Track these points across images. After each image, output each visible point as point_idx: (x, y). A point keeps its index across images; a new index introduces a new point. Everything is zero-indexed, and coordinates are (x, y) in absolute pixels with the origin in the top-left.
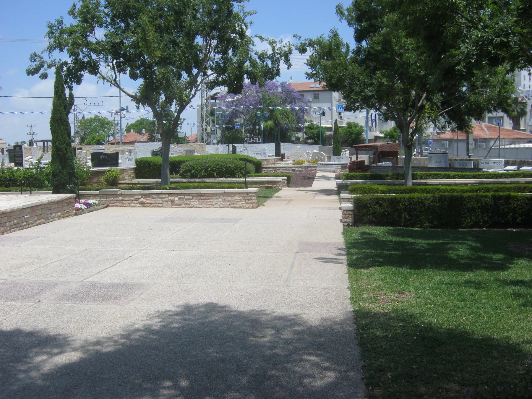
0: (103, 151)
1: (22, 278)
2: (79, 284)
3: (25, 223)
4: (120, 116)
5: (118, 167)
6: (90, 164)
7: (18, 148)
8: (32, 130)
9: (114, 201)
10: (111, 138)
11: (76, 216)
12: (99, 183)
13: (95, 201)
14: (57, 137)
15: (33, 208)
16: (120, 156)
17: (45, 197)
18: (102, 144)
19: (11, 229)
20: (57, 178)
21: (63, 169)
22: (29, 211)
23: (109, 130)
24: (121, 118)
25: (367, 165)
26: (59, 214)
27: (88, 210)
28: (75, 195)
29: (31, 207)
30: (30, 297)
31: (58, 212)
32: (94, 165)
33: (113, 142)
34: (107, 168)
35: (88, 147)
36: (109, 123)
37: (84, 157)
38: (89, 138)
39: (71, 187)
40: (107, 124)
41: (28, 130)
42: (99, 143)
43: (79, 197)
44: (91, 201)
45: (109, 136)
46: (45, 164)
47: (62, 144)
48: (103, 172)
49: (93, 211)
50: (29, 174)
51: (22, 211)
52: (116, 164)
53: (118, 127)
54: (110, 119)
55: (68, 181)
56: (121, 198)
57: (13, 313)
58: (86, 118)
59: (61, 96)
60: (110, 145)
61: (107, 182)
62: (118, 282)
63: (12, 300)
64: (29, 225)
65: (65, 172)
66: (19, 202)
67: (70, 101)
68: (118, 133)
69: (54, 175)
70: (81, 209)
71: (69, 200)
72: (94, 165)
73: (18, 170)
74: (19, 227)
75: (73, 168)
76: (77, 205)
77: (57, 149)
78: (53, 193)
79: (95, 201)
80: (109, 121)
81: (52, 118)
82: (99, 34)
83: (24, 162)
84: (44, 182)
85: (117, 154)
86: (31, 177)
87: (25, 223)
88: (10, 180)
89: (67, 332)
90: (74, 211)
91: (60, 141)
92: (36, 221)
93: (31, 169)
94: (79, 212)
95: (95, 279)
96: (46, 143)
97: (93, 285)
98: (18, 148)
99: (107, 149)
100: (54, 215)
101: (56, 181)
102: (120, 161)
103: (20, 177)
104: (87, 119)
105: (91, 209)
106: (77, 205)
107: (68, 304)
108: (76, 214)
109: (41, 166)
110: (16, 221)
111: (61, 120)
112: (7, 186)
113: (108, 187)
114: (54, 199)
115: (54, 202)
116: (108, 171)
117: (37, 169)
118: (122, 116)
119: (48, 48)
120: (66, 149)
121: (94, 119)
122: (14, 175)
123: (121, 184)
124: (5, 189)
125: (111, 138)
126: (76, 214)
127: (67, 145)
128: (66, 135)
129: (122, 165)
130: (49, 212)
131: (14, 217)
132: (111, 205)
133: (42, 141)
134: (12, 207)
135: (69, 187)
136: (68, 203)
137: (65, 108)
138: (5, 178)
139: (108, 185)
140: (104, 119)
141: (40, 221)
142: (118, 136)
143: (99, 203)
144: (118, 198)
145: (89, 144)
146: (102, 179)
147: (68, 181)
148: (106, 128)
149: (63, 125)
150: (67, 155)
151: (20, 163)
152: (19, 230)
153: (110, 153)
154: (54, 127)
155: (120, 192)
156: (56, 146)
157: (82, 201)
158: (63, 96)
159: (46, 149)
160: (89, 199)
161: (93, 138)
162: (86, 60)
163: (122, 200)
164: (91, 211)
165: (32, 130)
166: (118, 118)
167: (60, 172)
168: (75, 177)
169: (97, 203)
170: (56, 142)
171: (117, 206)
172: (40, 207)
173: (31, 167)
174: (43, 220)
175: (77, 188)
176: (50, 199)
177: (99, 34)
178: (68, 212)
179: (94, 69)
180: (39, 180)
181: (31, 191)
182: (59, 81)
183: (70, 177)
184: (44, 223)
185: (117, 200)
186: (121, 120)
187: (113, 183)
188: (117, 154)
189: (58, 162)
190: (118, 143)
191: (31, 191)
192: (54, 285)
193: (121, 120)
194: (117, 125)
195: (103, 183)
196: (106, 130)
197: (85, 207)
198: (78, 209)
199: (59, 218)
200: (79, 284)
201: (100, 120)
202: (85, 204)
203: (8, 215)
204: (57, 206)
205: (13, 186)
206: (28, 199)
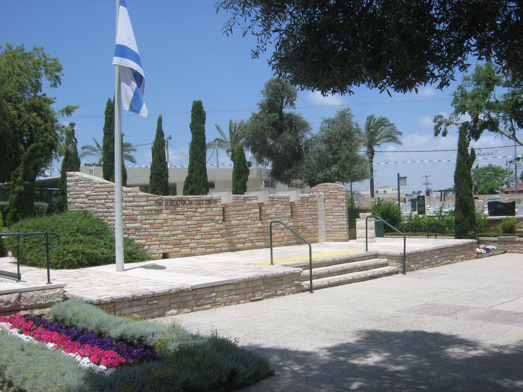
0: (499, 200)
1: (440, 302)
2: (486, 310)
3: (434, 262)
4: (516, 165)
5: (514, 215)
6: (486, 212)
7: (421, 198)
8: (427, 180)
9: (512, 248)
10: (505, 187)
11: (477, 260)
12: (496, 230)
13: (493, 247)
14: (460, 189)
15: (441, 250)
16: (516, 205)
17: (450, 241)
18: (496, 193)
19: (423, 267)
20: (460, 225)
21: (465, 217)
22: (437, 252)
23: (503, 178)
24: (516, 167)
25: (33, 204)
26: (463, 256)
27: (488, 254)
28: (476, 240)
29: (440, 249)
30: (450, 315)
31: (461, 255)
32: (491, 214)
33: (507, 190)
34: (504, 217)
35: (482, 196)
36: (503, 171)
37: (481, 205)
38: (482, 187)
39: (472, 234)
40: (501, 172)
41: (424, 180)
42: (492, 192)
43: (479, 242)
44: (490, 247)
45: (503, 185)
46: (445, 213)
47: (465, 195)
48: (500, 221)
49: (492, 255)
50: (433, 221)
51: (433, 251)
52: (513, 213)
53: (513, 176)
54: (504, 168)
55: (469, 228)
56: (518, 245)
57: (438, 323)
58: (479, 167)
59: (463, 152)
60: (504, 194)
61: (504, 230)
62: (520, 311)
63: (435, 315)
64: (437, 264)
65: (467, 219)
66: (429, 245)
67: (472, 157)
68: (512, 181)
69: (457, 222)
70: (481, 253)
71: (471, 245)
72: (491, 214)
73: (423, 218)
74: (429, 265)
75: (474, 216)
76: (478, 250)
77: (460, 199)
78: (455, 238)
79: (493, 247)
80: (503, 170)
81: (456, 173)
82: (500, 93)
83: (426, 211)
84: (445, 229)
85: (514, 203)
86: (434, 224)
87: (434, 262)
88: (417, 226)
89: (481, 339)
90: (475, 255)
91: (463, 192)
92: (443, 261)
93: (434, 217)
94: (479, 256)
95: (500, 308)
96: (443, 193)
97: (498, 312)
98: (421, 198)
99: (503, 198)
100: (458, 257)
101: (459, 227)
102: (516, 210)
103: (425, 223)
104: (481, 168)
105: (490, 253)
106: (478, 250)
107: (480, 322)
108: (477, 257)
109: (443, 214)
110: (427, 260)
111: (464, 174)
112: (415, 231)
113: (506, 234)
114: (458, 243)
115: (459, 246)
116: (505, 220)
117: (439, 217)
118: (518, 165)
119: (455, 112)
120: (468, 200)
121: (488, 168)
122: (420, 222)
123: (518, 232)
124: (413, 233)
125: (505, 187)
126: (477, 257)
127: (469, 196)
128: (468, 187)
129: (518, 214)
130: (454, 254)
131: (426, 257)
132: (508, 251)
133: (440, 191)
134: (424, 248)
135: (470, 233)
136: (471, 247)
137: (467, 163)
138: (412, 224)
139: (504, 233)
140: (498, 168)
141: (446, 261)
142: (513, 185)
143: (497, 249)
144: (515, 245)
145: (482, 193)
146: (499, 227)
147: (469, 228)
148: (500, 176)
149: (465, 178)
150: (469, 205)
151: (422, 211)
152: (430, 267)
153: (505, 202)
154: (458, 181)
155: (518, 239)
156: (459, 197)
157: (482, 246)
158: (465, 153)
159: (443, 198)
160: (488, 245)
161: (487, 186)
162: (486, 120)
163: (520, 247)
164: (490, 256)
165: (427, 180)
166: (512, 166)
167: (462, 220)
168: (475, 224)
169: (496, 248)
170: (459, 193)
171: (515, 252)
172: (447, 250)
173: (435, 215)
174: (449, 261)
175: (477, 234)
176: (455, 243)
177: (500, 93)
178: (470, 256)
179: (492, 126)
180: (441, 227)
181: (436, 236)
182: (462, 139)
183: (471, 225)
184: (449, 264)
185: (515, 247)
186: (516, 169)
187: (510, 230)
188: (514, 203)
189: (461, 211)
190: (513, 192)
191: (436, 236)
192: (466, 309)
193: (516, 169)
194: (512, 173)
195: (499, 231)
196: (500, 178)
197: (485, 252)
198: (478, 253)
199: (462, 259)
200: (486, 310)
201: (494, 168)
202: (484, 249)
203: (421, 255)
204: (460, 249)
205: (419, 232)
206: (436, 242)
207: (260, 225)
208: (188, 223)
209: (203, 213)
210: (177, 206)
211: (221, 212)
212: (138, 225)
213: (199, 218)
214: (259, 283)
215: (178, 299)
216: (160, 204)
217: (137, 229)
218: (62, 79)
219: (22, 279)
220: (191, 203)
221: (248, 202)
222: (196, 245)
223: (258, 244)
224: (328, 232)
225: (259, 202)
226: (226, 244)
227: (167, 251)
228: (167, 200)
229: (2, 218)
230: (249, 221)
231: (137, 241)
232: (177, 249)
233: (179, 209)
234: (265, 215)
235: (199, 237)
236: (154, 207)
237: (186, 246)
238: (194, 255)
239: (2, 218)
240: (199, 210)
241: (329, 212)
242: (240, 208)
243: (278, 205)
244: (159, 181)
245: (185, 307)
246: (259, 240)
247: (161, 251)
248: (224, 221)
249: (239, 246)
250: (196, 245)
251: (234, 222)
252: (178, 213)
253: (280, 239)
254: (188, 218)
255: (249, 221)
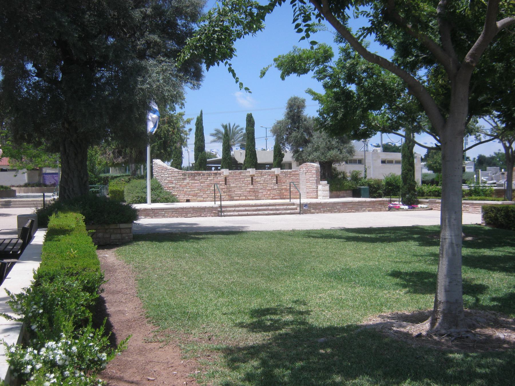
29: (343, 203)
74: (331, 211)
108: (389, 210)
207: (252, 187)
208: (202, 185)
209: (211, 180)
210: (194, 176)
211: (224, 180)
212: (174, 185)
213: (209, 183)
214: (190, 210)
215: (145, 213)
216: (185, 175)
217: (173, 187)
218: (185, 104)
219: (219, 358)
220: (204, 175)
221: (242, 174)
222: (207, 196)
223: (249, 198)
224: (307, 192)
225: (251, 174)
226: (227, 197)
227: (189, 198)
228: (188, 173)
229: (388, 48)
230: (243, 185)
231: (173, 193)
232: (195, 198)
233: (196, 178)
234: (255, 182)
235: (209, 192)
236: (182, 177)
237: (199, 196)
238: (206, 201)
239: (388, 48)
240: (209, 178)
241: (308, 181)
242: (237, 177)
243: (266, 176)
244: (203, 162)
245: (148, 216)
246: (251, 196)
247: (186, 198)
248: (226, 184)
249: (235, 198)
250: (207, 196)
251: (232, 185)
252: (196, 180)
253: (268, 196)
254: (201, 183)
255: (243, 185)
